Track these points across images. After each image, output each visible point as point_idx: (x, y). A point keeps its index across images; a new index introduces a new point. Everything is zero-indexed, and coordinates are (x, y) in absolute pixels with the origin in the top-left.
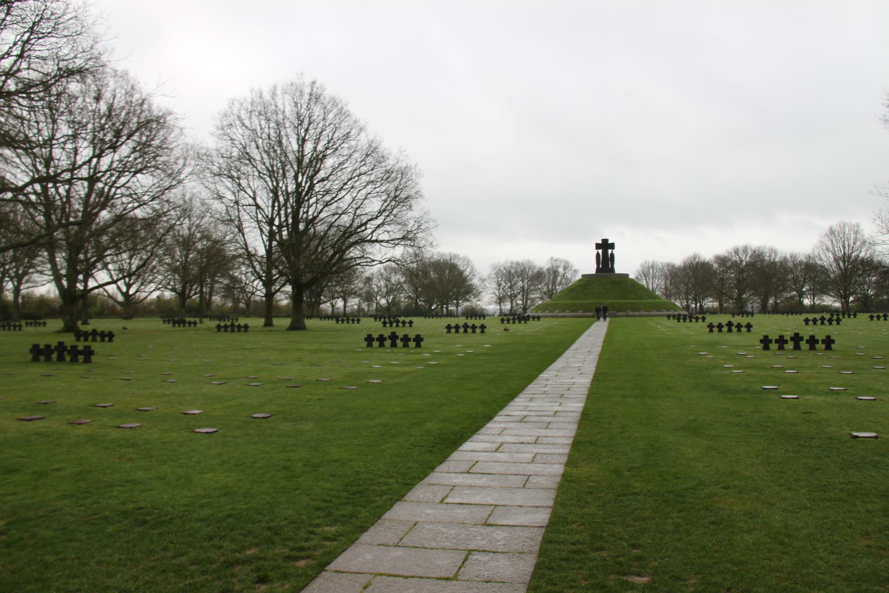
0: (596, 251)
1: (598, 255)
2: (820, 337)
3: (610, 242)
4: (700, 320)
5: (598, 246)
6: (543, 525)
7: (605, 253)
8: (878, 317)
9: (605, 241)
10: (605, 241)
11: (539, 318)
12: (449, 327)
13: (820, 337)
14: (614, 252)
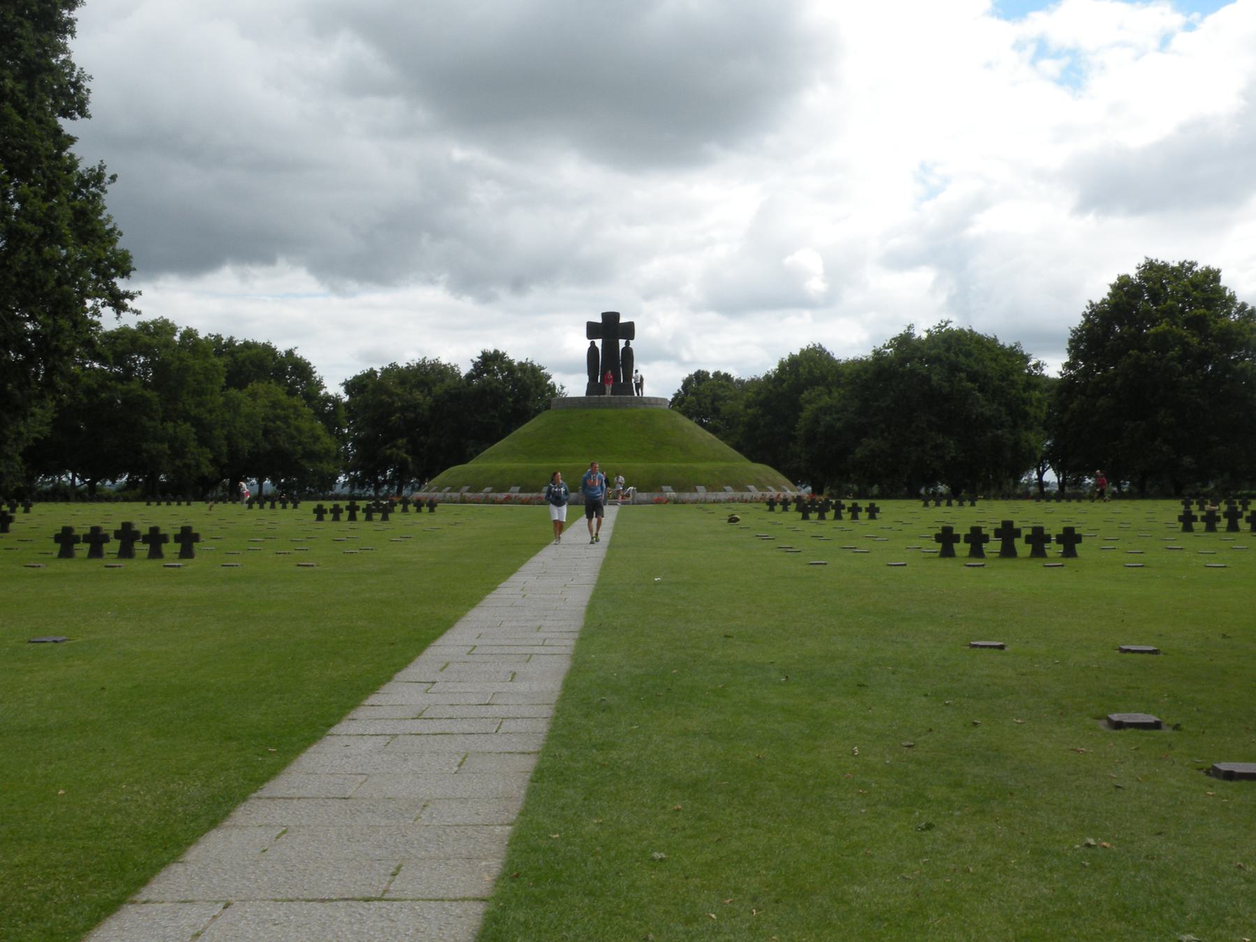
0: (587, 343)
1: (592, 350)
2: (1054, 528)
3: (622, 320)
4: (863, 515)
5: (593, 331)
6: (486, 894)
7: (610, 347)
8: (1211, 521)
9: (611, 319)
10: (611, 319)
11: (432, 505)
12: (66, 540)
13: (1054, 528)
14: (632, 344)
